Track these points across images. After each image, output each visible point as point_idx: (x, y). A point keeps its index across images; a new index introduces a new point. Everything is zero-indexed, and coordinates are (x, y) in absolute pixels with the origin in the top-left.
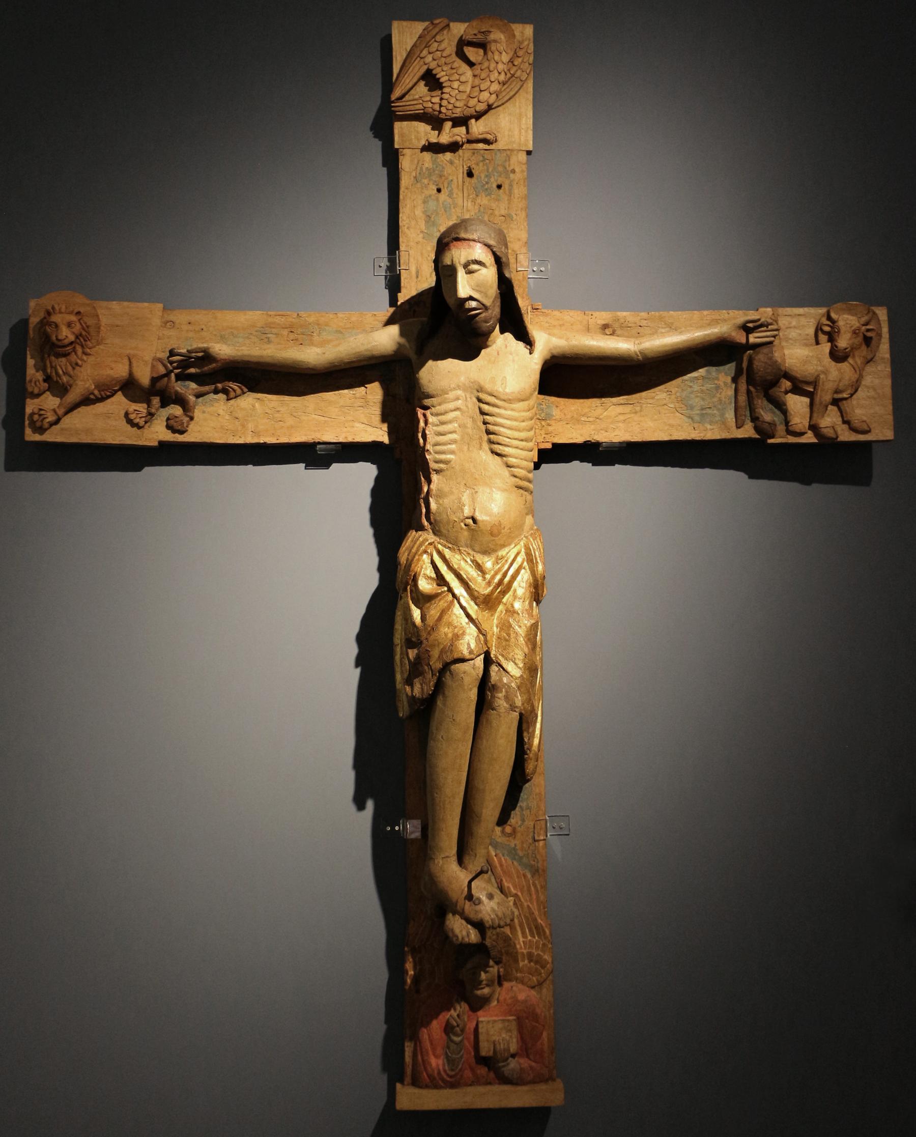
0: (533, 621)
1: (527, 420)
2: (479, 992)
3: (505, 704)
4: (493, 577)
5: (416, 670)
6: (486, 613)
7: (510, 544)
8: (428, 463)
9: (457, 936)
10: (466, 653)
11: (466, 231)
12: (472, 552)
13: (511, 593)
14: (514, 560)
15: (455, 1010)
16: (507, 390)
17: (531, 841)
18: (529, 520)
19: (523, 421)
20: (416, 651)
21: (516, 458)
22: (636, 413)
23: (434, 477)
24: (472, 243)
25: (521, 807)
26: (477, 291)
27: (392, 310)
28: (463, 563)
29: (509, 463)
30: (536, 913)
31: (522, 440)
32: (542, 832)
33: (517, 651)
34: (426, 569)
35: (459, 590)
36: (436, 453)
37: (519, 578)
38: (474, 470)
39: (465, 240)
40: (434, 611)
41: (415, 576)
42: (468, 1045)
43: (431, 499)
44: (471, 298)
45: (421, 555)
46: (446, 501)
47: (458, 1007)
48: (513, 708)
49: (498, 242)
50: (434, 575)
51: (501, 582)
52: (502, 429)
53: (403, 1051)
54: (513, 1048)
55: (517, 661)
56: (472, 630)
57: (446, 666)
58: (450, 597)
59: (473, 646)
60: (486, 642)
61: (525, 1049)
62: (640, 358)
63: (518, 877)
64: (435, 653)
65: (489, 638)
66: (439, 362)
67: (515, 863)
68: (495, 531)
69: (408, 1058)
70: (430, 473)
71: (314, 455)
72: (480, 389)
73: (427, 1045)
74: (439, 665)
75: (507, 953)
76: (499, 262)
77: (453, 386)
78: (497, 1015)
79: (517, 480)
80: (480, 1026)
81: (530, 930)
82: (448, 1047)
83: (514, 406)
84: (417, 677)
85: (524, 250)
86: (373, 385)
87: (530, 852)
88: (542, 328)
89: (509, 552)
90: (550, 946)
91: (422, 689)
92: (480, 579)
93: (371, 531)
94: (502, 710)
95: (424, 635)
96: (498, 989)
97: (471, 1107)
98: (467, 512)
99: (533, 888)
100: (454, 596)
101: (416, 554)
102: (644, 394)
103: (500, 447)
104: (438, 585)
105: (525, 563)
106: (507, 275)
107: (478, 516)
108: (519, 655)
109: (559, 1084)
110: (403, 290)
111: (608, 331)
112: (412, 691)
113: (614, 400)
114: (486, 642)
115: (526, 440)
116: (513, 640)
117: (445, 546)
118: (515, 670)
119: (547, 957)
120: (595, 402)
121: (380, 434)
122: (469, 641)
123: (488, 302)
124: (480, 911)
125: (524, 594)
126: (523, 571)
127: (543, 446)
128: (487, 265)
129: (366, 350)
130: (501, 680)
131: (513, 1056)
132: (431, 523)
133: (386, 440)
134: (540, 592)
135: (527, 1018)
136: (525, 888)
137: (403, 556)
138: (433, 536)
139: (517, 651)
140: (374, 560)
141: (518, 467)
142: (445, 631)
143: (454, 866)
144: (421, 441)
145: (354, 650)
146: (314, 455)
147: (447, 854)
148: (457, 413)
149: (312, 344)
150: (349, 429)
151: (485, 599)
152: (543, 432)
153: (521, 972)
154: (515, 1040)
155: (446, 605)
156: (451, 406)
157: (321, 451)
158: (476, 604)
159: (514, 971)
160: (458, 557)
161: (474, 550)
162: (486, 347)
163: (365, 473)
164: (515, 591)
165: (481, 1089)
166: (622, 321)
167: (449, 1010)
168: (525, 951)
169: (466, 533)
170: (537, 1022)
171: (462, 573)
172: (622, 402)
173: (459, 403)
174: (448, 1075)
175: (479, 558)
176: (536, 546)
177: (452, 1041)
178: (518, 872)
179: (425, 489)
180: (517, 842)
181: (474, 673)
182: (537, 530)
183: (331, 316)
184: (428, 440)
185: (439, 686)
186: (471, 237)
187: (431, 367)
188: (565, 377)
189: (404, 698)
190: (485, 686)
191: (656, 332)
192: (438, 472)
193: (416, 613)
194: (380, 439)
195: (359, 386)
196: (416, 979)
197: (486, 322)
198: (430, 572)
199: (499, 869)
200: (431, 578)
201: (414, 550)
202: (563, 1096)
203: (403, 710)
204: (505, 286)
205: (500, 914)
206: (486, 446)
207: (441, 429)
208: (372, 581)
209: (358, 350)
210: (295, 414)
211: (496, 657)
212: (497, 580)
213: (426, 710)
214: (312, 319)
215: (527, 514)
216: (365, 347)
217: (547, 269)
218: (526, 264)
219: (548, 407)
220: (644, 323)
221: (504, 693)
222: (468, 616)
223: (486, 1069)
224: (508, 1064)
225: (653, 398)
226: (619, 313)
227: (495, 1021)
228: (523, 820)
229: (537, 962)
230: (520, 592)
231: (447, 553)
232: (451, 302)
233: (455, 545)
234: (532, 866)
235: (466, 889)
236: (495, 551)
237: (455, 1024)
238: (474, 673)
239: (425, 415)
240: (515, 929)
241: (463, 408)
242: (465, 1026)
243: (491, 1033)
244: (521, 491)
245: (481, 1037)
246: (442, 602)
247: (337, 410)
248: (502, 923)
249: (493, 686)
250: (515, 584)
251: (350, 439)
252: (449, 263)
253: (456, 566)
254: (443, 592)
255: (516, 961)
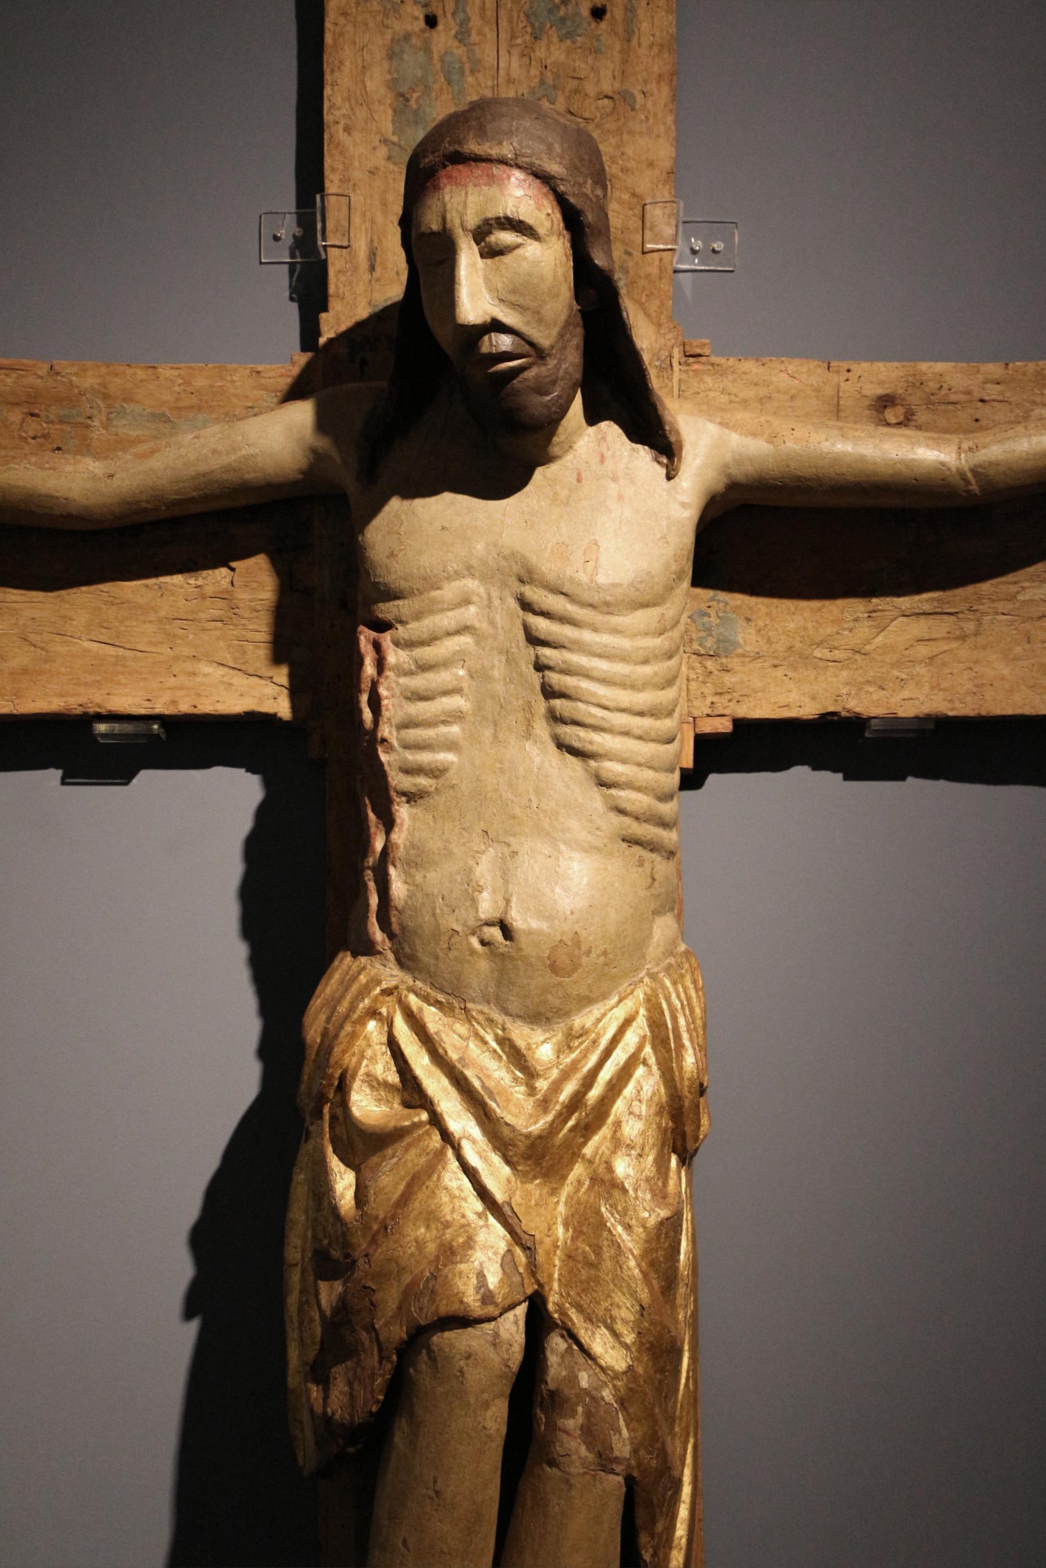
0: (664, 1213)
1: (657, 660)
3: (583, 1451)
4: (556, 1087)
5: (340, 1335)
6: (535, 1188)
7: (604, 996)
8: (384, 775)
10: (471, 1299)
11: (482, 133)
12: (498, 1017)
13: (605, 1131)
14: (615, 1041)
16: (601, 579)
18: (664, 928)
19: (646, 662)
20: (338, 1287)
21: (624, 761)
22: (963, 638)
23: (403, 812)
24: (497, 170)
26: (514, 306)
27: (303, 359)
28: (473, 1048)
29: (605, 775)
31: (641, 714)
33: (619, 1298)
34: (373, 1059)
35: (460, 1121)
36: (406, 746)
37: (629, 1090)
38: (508, 795)
39: (478, 159)
40: (390, 1176)
41: (342, 1078)
43: (392, 871)
44: (496, 326)
45: (362, 1021)
46: (433, 878)
48: (605, 1461)
49: (573, 168)
50: (393, 1078)
51: (577, 1101)
52: (585, 684)
55: (619, 1327)
56: (493, 1237)
57: (419, 1336)
58: (435, 1140)
59: (493, 1280)
60: (533, 1267)
62: (974, 487)
64: (390, 1297)
65: (541, 1257)
66: (419, 502)
68: (563, 960)
70: (390, 802)
71: (87, 749)
72: (527, 576)
74: (399, 1332)
76: (573, 221)
77: (453, 566)
79: (627, 821)
83: (616, 620)
84: (339, 1360)
85: (665, 193)
86: (251, 562)
88: (709, 410)
89: (605, 1017)
91: (352, 1397)
92: (519, 1092)
93: (241, 950)
94: (576, 1469)
95: (361, 1242)
98: (487, 906)
100: (447, 1136)
101: (347, 1017)
102: (986, 587)
103: (582, 733)
104: (407, 1105)
105: (648, 1049)
106: (599, 260)
107: (518, 920)
108: (625, 1312)
110: (335, 305)
111: (890, 415)
112: (326, 1398)
113: (905, 602)
114: (533, 1267)
115: (653, 713)
116: (608, 1264)
117: (426, 999)
118: (610, 1351)
120: (853, 608)
121: (269, 695)
122: (487, 1261)
123: (544, 338)
125: (643, 1133)
126: (640, 1071)
127: (708, 727)
128: (541, 231)
129: (226, 469)
130: (572, 1379)
132: (391, 936)
133: (283, 708)
134: (688, 1129)
137: (314, 1026)
138: (396, 971)
139: (619, 1298)
140: (250, 1027)
141: (630, 785)
142: (417, 1236)
144: (367, 715)
145: (182, 1269)
146: (87, 749)
148: (465, 641)
149: (85, 448)
150: (182, 679)
151: (532, 1146)
152: (709, 689)
155: (422, 1160)
156: (447, 620)
157: (105, 736)
158: (508, 1162)
160: (461, 1028)
161: (506, 1012)
162: (547, 459)
163: (233, 795)
164: (618, 1124)
166: (933, 385)
169: (484, 965)
171: (469, 1073)
172: (927, 607)
173: (471, 614)
175: (521, 1034)
176: (683, 1002)
179: (379, 845)
181: (494, 1357)
182: (687, 953)
183: (141, 374)
184: (386, 714)
185: (399, 1391)
186: (494, 152)
187: (397, 516)
188: (762, 540)
189: (306, 1417)
190: (529, 1391)
191: (1026, 417)
192: (412, 797)
193: (344, 1182)
194: (267, 707)
195: (214, 566)
197: (541, 391)
198: (384, 1069)
200: (386, 1085)
201: (342, 1009)
203: (307, 1452)
204: (596, 296)
206: (542, 729)
207: (419, 682)
208: (243, 1082)
209: (202, 468)
210: (32, 637)
211: (563, 1312)
212: (564, 1096)
213: (366, 1450)
214: (89, 381)
215: (657, 912)
216: (224, 460)
217: (730, 246)
218: (669, 231)
219: (724, 620)
220: (993, 391)
221: (580, 1419)
222: (483, 1193)
225: (1012, 598)
226: (924, 366)
230: (632, 1129)
231: (432, 1017)
232: (443, 335)
233: (453, 997)
236: (564, 1014)
238: (494, 1357)
239: (377, 646)
241: (483, 626)
244: (637, 850)
246: (413, 1152)
247: (150, 628)
249: (553, 1394)
250: (619, 1106)
251: (185, 707)
252: (435, 227)
253: (453, 1056)
254: (416, 1126)
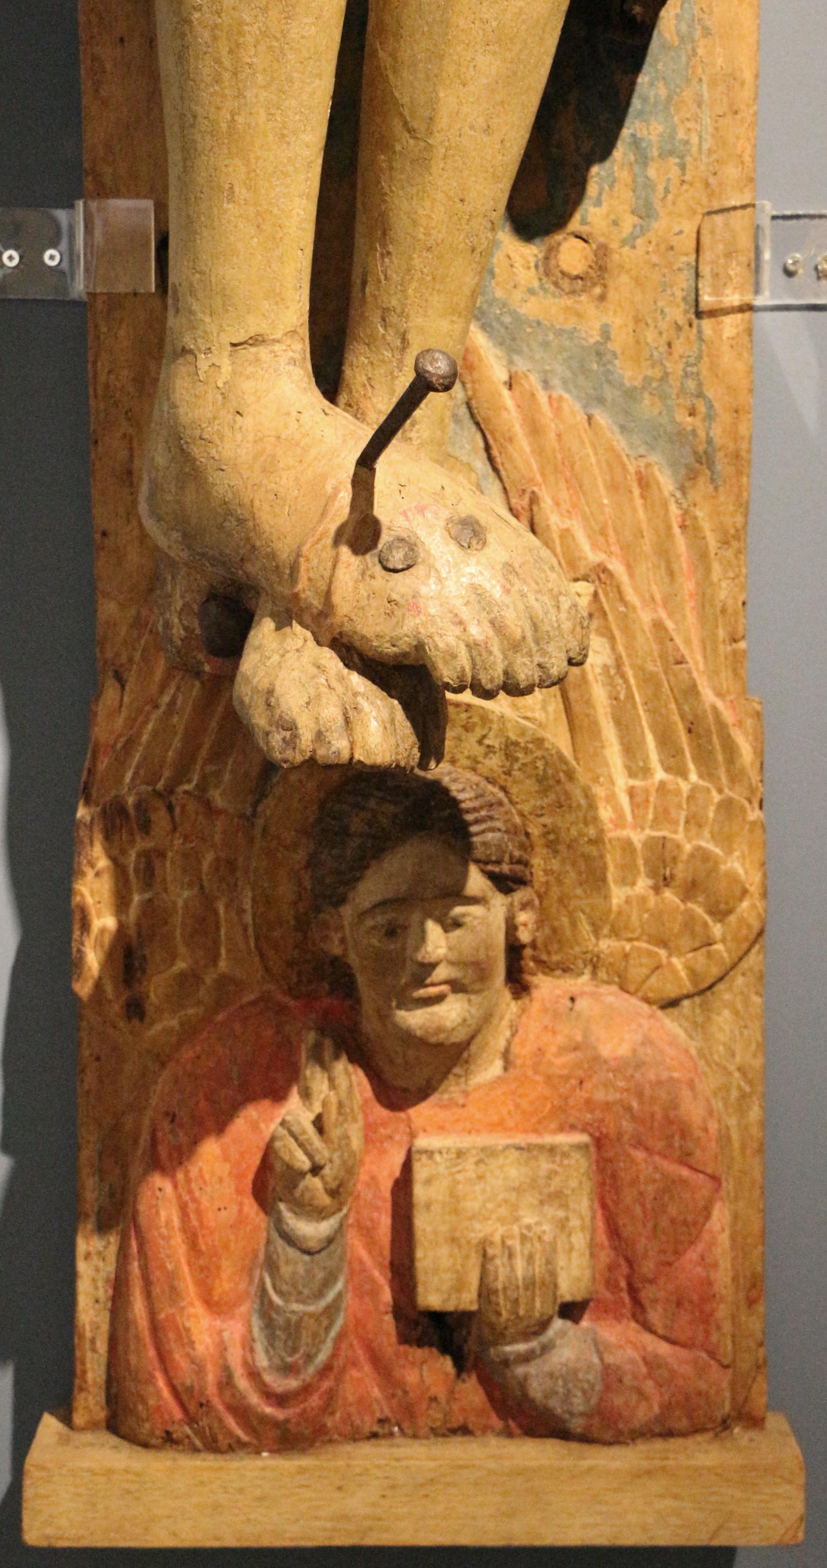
2: (414, 1019)
9: (291, 727)
15: (306, 1095)
17: (679, 313)
25: (636, 142)
30: (696, 662)
32: (736, 270)
42: (369, 1257)
47: (319, 1083)
53: (70, 1277)
54: (574, 1275)
61: (626, 1287)
63: (613, 487)
67: (602, 418)
69: (90, 1310)
73: (173, 1250)
75: (553, 841)
78: (499, 1126)
80: (421, 1171)
81: (665, 740)
82: (271, 1265)
87: (675, 368)
90: (754, 814)
96: (509, 1007)
97: (372, 1540)
99: (681, 542)
109: (777, 1445)
119: (739, 865)
124: (414, 604)
131: (571, 1311)
135: (639, 1143)
136: (647, 545)
143: (283, 379)
147: (254, 326)
153: (615, 932)
154: (580, 1240)
159: (585, 927)
165: (419, 1456)
167: (278, 1096)
168: (637, 838)
170: (685, 1158)
174: (268, 1395)
177: (289, 1239)
178: (614, 461)
180: (617, 321)
196: (127, 957)
199: (523, 443)
202: (799, 1507)
205: (517, 625)
223: (448, 1364)
224: (546, 1349)
227: (489, 1152)
228: (645, 212)
229: (690, 890)
234: (680, 436)
235: (345, 496)
237: (302, 1161)
240: (595, 732)
242: (350, 1170)
243: (472, 1205)
245: (422, 1223)
248: (524, 673)
255: (595, 879)
